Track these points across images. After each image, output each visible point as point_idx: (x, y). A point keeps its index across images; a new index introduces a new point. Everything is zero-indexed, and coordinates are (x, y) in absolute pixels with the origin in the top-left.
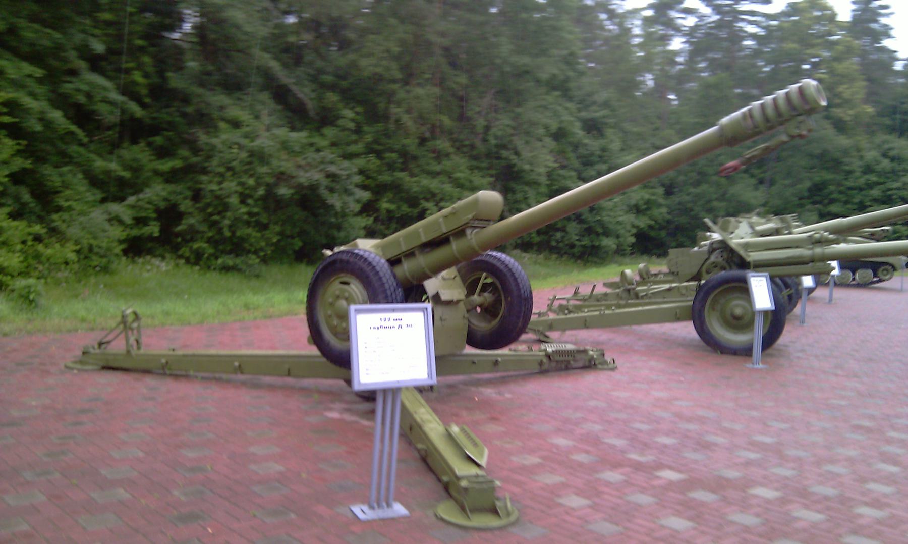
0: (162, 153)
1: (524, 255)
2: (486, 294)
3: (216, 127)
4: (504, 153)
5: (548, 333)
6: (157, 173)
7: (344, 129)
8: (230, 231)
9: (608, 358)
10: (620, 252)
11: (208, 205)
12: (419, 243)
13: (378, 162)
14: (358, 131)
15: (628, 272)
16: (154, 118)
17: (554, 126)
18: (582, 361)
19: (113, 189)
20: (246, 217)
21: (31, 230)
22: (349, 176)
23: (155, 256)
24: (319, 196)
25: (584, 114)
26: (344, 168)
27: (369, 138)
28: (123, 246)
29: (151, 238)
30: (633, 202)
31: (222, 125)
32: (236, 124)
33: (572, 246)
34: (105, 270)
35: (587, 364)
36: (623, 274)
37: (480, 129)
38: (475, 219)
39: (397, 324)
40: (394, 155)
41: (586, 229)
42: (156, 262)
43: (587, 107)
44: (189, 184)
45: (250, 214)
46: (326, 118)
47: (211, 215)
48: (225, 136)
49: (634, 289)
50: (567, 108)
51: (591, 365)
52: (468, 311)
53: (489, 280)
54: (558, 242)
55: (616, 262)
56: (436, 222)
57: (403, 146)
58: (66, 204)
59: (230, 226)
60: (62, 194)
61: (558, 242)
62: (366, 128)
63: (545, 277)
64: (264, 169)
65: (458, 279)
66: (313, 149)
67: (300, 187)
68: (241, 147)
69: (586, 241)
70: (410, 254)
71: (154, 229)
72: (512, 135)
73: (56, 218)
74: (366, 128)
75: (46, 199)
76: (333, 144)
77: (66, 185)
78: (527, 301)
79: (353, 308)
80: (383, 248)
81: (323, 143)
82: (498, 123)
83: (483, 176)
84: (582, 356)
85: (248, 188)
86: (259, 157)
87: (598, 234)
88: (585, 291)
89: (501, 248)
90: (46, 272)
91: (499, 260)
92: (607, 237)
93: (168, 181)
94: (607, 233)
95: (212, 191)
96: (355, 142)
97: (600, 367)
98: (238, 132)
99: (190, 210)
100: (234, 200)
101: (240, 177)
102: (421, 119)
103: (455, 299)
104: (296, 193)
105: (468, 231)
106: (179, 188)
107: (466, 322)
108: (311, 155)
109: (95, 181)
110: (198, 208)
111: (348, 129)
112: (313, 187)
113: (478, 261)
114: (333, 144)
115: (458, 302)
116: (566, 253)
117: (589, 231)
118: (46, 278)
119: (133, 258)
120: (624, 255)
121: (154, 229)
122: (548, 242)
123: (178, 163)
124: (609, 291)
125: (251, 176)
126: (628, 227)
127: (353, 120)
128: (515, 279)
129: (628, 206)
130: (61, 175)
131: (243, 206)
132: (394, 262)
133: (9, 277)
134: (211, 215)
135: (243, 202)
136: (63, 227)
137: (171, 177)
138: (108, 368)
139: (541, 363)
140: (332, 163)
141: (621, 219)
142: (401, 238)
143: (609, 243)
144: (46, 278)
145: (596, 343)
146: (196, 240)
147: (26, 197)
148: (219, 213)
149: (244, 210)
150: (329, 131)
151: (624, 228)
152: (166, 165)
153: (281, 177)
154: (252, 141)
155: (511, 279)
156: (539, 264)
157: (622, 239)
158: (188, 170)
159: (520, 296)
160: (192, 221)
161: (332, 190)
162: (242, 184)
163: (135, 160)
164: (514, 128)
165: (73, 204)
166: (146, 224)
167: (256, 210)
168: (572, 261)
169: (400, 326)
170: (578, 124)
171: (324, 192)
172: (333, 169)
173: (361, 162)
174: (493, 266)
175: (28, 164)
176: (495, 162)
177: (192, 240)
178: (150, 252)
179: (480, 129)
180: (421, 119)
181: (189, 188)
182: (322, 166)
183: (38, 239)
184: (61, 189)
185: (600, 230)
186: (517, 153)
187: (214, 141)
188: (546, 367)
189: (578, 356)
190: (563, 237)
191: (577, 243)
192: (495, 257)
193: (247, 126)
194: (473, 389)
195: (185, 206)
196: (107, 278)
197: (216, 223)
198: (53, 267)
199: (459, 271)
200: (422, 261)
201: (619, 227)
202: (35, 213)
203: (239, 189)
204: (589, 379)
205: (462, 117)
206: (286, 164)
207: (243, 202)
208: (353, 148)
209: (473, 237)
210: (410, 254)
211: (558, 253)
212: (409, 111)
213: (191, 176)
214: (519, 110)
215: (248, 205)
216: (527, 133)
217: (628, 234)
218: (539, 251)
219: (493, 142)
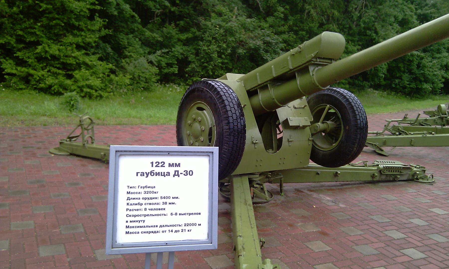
0: (183, 30)
1: (375, 91)
2: (329, 122)
3: (210, 16)
4: (369, 32)
5: (383, 148)
6: (179, 40)
7: (277, 18)
8: (212, 72)
9: (428, 174)
10: (434, 92)
11: (202, 58)
12: (271, 78)
13: (295, 37)
14: (286, 19)
15: (443, 106)
16: (181, 12)
17: (400, 18)
18: (406, 175)
19: (151, 46)
20: (220, 64)
21: (107, 66)
22: (276, 43)
23: (175, 84)
24: (259, 54)
25: (419, 11)
26: (273, 39)
27: (291, 23)
28: (158, 77)
29: (174, 74)
30: (445, 63)
31: (213, 15)
32: (220, 14)
33: (404, 87)
34: (146, 89)
35: (411, 178)
36: (439, 107)
37: (355, 18)
38: (316, 57)
39: (172, 170)
40: (304, 33)
41: (414, 78)
42: (175, 86)
43: (421, 8)
44: (195, 46)
45: (223, 63)
46: (270, 12)
47: (203, 63)
48: (215, 20)
49: (446, 117)
50: (409, 8)
51: (414, 179)
52: (313, 135)
53: (332, 111)
54: (396, 85)
55: (431, 98)
56: (286, 60)
57: (310, 27)
58: (129, 54)
59: (212, 70)
60: (127, 49)
61: (396, 85)
62: (290, 17)
63: (386, 105)
64: (231, 39)
65: (307, 108)
66: (260, 29)
67: (250, 49)
68: (220, 27)
69: (413, 85)
70: (264, 87)
71: (175, 70)
72: (374, 22)
73: (123, 62)
74: (290, 17)
75: (119, 50)
76: (271, 26)
77: (130, 44)
78: (363, 129)
79: (113, 148)
80: (244, 81)
81: (266, 25)
82: (367, 14)
83: (355, 46)
84: (408, 172)
85: (223, 49)
86: (230, 32)
87: (421, 81)
88: (412, 117)
89: (339, 84)
90: (114, 89)
91: (342, 94)
92: (426, 83)
93: (184, 45)
94: (427, 81)
95: (204, 50)
96: (283, 25)
97: (421, 180)
98: (220, 19)
99: (194, 60)
100: (215, 55)
101: (219, 43)
102: (323, 13)
103: (301, 125)
104: (247, 52)
105: (311, 69)
106: (190, 48)
107: (311, 143)
108: (259, 31)
109: (146, 43)
110: (197, 59)
111: (281, 18)
112: (256, 49)
113: (324, 95)
114: (271, 26)
115: (304, 127)
116: (400, 92)
117: (416, 79)
118: (113, 92)
119: (165, 84)
120: (435, 94)
121: (175, 70)
122: (391, 84)
123: (190, 35)
124: (428, 117)
125: (224, 42)
126: (440, 78)
127: (282, 13)
128: (354, 111)
129: (441, 66)
130: (128, 39)
131: (219, 59)
132: (251, 93)
133: (94, 91)
134: (203, 63)
135: (220, 56)
136: (126, 66)
137: (186, 43)
138: (71, 154)
139: (373, 176)
140: (268, 36)
141: (436, 73)
142: (259, 74)
143: (427, 86)
144: (113, 92)
145: (419, 158)
146: (195, 76)
147: (109, 50)
148: (207, 63)
149: (220, 60)
150: (270, 19)
151: (437, 78)
152: (184, 37)
153: (241, 43)
154: (227, 24)
155: (350, 111)
156: (384, 97)
157: (435, 85)
158: (195, 39)
159: (356, 125)
160: (194, 66)
161: (267, 51)
162: (219, 47)
163: (168, 33)
164: (376, 18)
165: (132, 54)
166: (172, 67)
167: (226, 61)
168: (404, 96)
169: (177, 174)
170: (415, 17)
171: (262, 51)
172: (268, 39)
173: (285, 36)
174: (337, 99)
175: (110, 32)
176: (363, 37)
177: (193, 76)
178: (173, 82)
179: (355, 18)
180: (323, 13)
181: (195, 49)
182: (262, 38)
183: (113, 72)
184: (127, 46)
185: (423, 79)
186: (376, 33)
187: (208, 23)
188: (377, 179)
189: (404, 172)
190: (399, 82)
191: (407, 85)
192: (339, 92)
193: (225, 15)
194: (315, 195)
195: (192, 58)
196: (146, 93)
197: (206, 67)
198: (118, 87)
199: (308, 102)
200: (273, 93)
201: (434, 78)
202: (114, 58)
203: (218, 49)
204: (411, 190)
205: (346, 12)
206: (243, 36)
207: (220, 56)
208: (282, 29)
209: (315, 74)
210: (264, 87)
211: (395, 91)
212: (315, 7)
213: (196, 42)
214: (379, 7)
215: (222, 58)
216: (383, 21)
217: (439, 82)
218: (384, 90)
219: (363, 25)
